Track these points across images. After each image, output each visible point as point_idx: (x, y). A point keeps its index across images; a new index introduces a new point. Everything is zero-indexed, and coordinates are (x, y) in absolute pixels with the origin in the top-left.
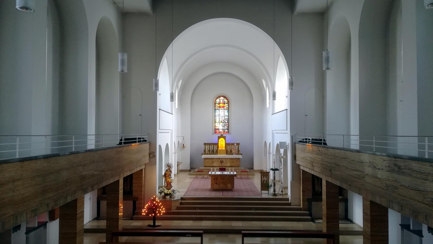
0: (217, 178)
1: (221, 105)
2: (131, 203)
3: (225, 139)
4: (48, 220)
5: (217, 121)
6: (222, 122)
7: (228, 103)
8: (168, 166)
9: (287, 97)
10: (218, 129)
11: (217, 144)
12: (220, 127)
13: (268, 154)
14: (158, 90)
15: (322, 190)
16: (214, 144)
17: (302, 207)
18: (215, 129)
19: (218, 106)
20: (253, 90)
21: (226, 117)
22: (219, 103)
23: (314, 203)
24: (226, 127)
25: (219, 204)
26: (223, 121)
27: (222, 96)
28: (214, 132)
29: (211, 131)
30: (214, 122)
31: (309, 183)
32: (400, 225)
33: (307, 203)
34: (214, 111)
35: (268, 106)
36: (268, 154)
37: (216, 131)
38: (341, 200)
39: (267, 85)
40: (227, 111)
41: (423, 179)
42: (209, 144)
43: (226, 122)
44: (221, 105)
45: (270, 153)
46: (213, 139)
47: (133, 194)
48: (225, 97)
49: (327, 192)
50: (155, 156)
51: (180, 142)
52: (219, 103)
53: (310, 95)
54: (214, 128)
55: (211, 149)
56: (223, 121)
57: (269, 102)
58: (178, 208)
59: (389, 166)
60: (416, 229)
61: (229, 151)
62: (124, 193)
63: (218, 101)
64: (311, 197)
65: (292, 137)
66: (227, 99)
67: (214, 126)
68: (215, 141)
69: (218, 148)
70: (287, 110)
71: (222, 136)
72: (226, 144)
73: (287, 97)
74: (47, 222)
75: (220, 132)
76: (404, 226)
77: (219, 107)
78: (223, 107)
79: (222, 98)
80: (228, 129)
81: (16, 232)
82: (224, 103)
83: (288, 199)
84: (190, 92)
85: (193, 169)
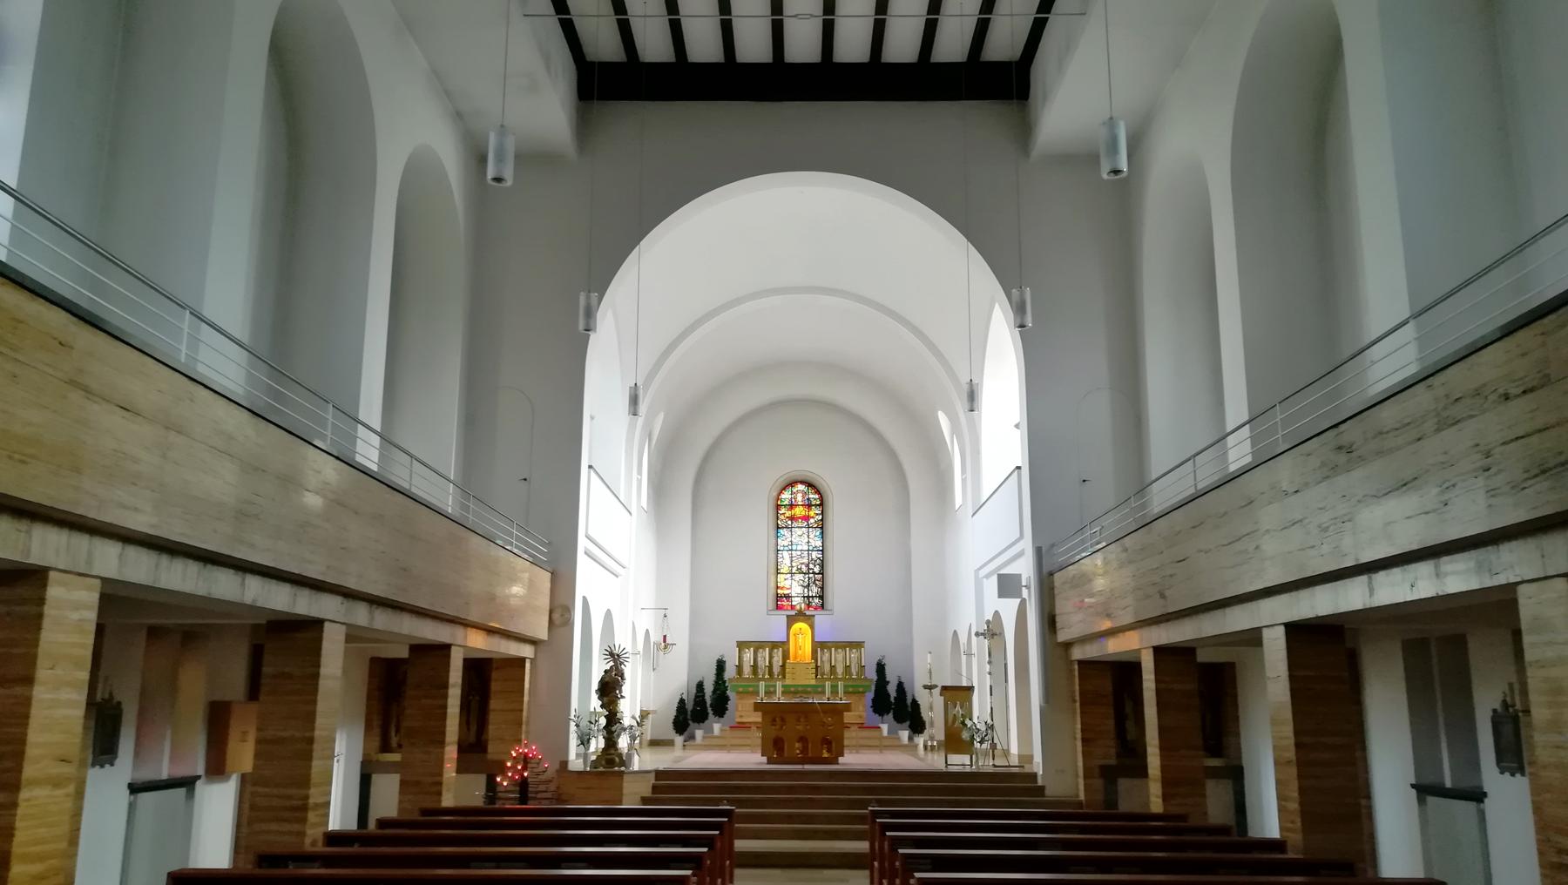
0: (783, 720)
1: (799, 511)
2: (481, 780)
3: (812, 627)
4: (200, 770)
5: (785, 569)
6: (800, 571)
7: (821, 505)
8: (612, 654)
9: (1017, 426)
10: (788, 597)
11: (783, 645)
12: (794, 587)
13: (964, 658)
14: (595, 330)
15: (1149, 701)
16: (774, 645)
17: (1082, 797)
18: (778, 597)
19: (788, 514)
20: (906, 454)
21: (814, 555)
22: (792, 506)
23: (1124, 784)
24: (815, 590)
25: (790, 789)
26: (804, 569)
27: (802, 482)
28: (772, 605)
29: (765, 600)
30: (773, 570)
31: (1098, 692)
32: (1413, 786)
33: (1098, 783)
34: (773, 533)
35: (958, 500)
36: (964, 658)
37: (780, 601)
38: (1215, 773)
39: (956, 429)
40: (818, 532)
41: (1410, 443)
42: (758, 646)
43: (817, 569)
44: (799, 511)
45: (969, 655)
46: (774, 626)
47: (490, 748)
48: (810, 485)
49: (1158, 692)
50: (568, 623)
51: (652, 639)
52: (792, 506)
53: (1096, 414)
54: (772, 591)
55: (760, 663)
56: (804, 569)
57: (964, 481)
58: (645, 800)
59: (1323, 464)
60: (1466, 784)
61: (827, 668)
62: (463, 749)
63: (786, 496)
64: (1113, 762)
65: (1039, 553)
66: (818, 492)
67: (773, 585)
68: (779, 636)
69: (786, 656)
70: (1019, 468)
71: (800, 616)
72: (818, 646)
73: (1017, 426)
74: (199, 777)
75: (793, 607)
76: (1425, 790)
77: (792, 518)
78: (806, 518)
79: (801, 487)
80: (821, 597)
81: (102, 766)
82: (809, 506)
83: (1035, 775)
84: (688, 473)
85: (696, 710)
